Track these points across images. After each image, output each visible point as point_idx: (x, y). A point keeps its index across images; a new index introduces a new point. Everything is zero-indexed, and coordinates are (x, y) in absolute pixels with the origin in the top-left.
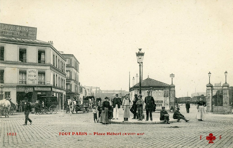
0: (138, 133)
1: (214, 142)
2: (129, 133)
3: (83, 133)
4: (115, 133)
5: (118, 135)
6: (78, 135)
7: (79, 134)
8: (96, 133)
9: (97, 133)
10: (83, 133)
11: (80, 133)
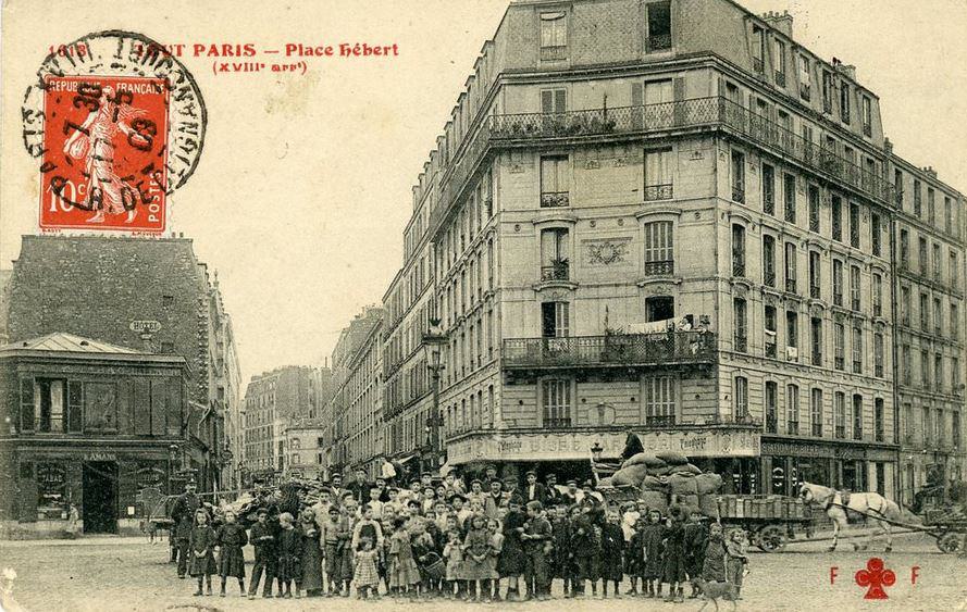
0: (275, 63)
1: (888, 590)
2: (237, 65)
3: (238, 47)
4: (352, 47)
5: (386, 53)
6: (217, 54)
7: (220, 50)
8: (295, 48)
9: (301, 46)
10: (238, 47)
11: (224, 46)
